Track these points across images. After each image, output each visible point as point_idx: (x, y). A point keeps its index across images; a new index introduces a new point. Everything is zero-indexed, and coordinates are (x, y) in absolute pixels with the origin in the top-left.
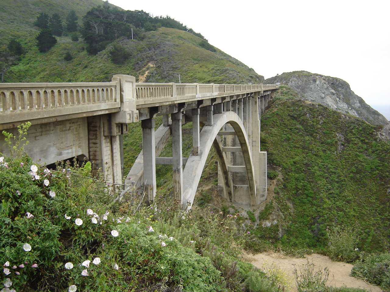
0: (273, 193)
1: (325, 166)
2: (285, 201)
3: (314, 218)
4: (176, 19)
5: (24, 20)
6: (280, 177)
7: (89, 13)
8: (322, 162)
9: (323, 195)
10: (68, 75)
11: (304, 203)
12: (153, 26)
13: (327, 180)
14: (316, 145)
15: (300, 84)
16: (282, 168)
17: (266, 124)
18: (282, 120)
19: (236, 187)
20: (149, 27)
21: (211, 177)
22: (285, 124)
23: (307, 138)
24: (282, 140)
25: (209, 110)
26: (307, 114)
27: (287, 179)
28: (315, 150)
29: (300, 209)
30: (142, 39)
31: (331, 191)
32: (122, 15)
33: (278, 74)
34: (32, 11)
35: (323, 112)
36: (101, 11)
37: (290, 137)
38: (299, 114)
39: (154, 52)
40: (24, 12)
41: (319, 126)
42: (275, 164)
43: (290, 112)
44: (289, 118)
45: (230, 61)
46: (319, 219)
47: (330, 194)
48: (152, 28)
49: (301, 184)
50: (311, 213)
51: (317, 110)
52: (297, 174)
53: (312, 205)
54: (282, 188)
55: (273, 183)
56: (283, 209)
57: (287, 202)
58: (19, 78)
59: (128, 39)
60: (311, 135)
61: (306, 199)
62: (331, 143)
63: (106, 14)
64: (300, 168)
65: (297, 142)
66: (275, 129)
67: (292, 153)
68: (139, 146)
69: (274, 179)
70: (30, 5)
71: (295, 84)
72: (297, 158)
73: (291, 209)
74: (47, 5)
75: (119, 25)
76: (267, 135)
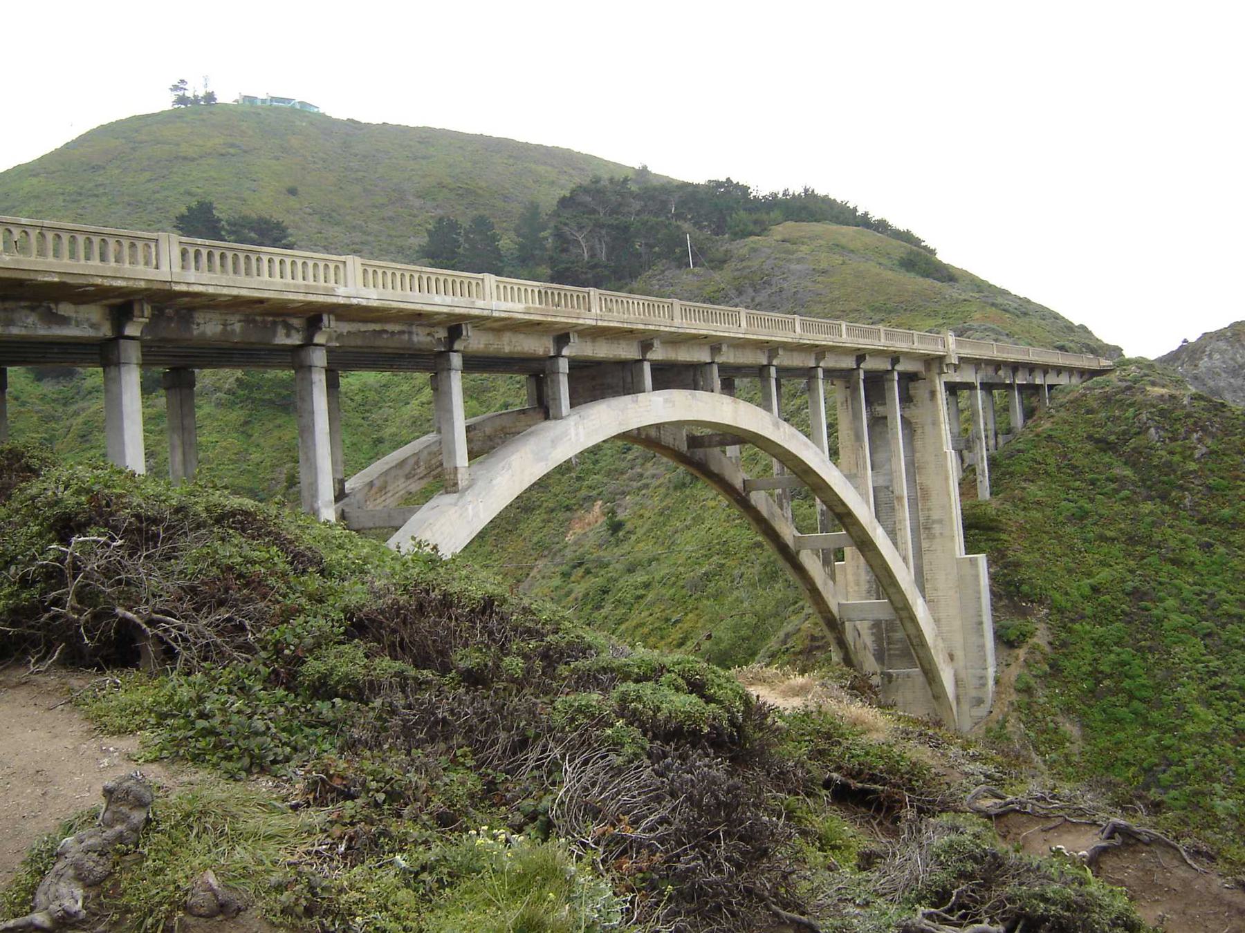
0: (1012, 690)
1: (1204, 597)
2: (1054, 715)
3: (1148, 771)
4: (838, 195)
5: (389, 244)
6: (1041, 638)
7: (564, 202)
8: (1195, 584)
9: (1187, 691)
10: (502, 390)
11: (1118, 721)
12: (756, 222)
13: (1208, 641)
14: (1176, 529)
15: (1239, 359)
16: (1050, 609)
17: (1010, 470)
18: (1065, 456)
19: (890, 676)
20: (741, 226)
21: (818, 648)
22: (1074, 467)
23: (1147, 507)
24: (1061, 518)
25: (554, 373)
26: (1149, 428)
27: (1064, 644)
28: (1172, 543)
29: (1104, 742)
30: (719, 263)
31: (1218, 680)
32: (664, 197)
33: (1185, 341)
34: (415, 216)
35: (1209, 420)
36: (598, 191)
37: (1088, 506)
38: (1124, 433)
39: (753, 300)
40: (391, 219)
41: (1192, 466)
42: (1027, 597)
43: (1094, 426)
44: (1089, 446)
45: (993, 305)
46: (1164, 771)
47: (1214, 688)
48: (751, 227)
49: (1112, 656)
50: (1141, 754)
51: (1185, 412)
52: (1101, 624)
53: (1147, 725)
54: (1046, 673)
55: (1017, 658)
56: (1043, 743)
57: (1060, 719)
58: (362, 408)
59: (679, 267)
60: (1164, 497)
61: (1127, 706)
62: (1233, 518)
63: (613, 198)
64: (1113, 607)
65: (1112, 521)
66: (1040, 486)
67: (1089, 559)
68: (683, 587)
69: (1019, 647)
70: (411, 198)
71: (1224, 362)
72: (1104, 575)
73: (1072, 743)
74: (461, 195)
75: (652, 227)
76: (1008, 506)
